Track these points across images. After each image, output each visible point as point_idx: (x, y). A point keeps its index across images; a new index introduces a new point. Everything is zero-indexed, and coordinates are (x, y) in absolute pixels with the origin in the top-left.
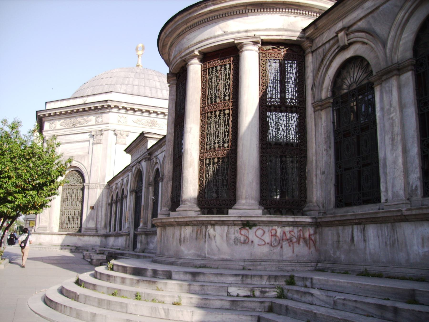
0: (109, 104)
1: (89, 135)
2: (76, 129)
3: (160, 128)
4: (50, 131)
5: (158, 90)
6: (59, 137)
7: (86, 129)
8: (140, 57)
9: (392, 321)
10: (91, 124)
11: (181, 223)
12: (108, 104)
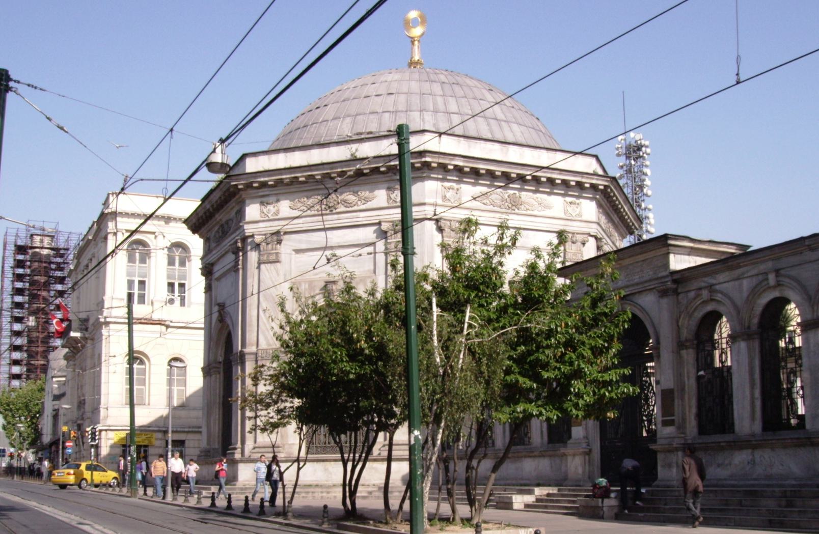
0: (428, 159)
1: (375, 232)
2: (336, 216)
3: (529, 212)
4: (263, 221)
5: (503, 123)
6: (286, 237)
7: (362, 218)
8: (416, 43)
9: (2, 287)
10: (375, 206)
11: (215, 316)
12: (423, 160)
